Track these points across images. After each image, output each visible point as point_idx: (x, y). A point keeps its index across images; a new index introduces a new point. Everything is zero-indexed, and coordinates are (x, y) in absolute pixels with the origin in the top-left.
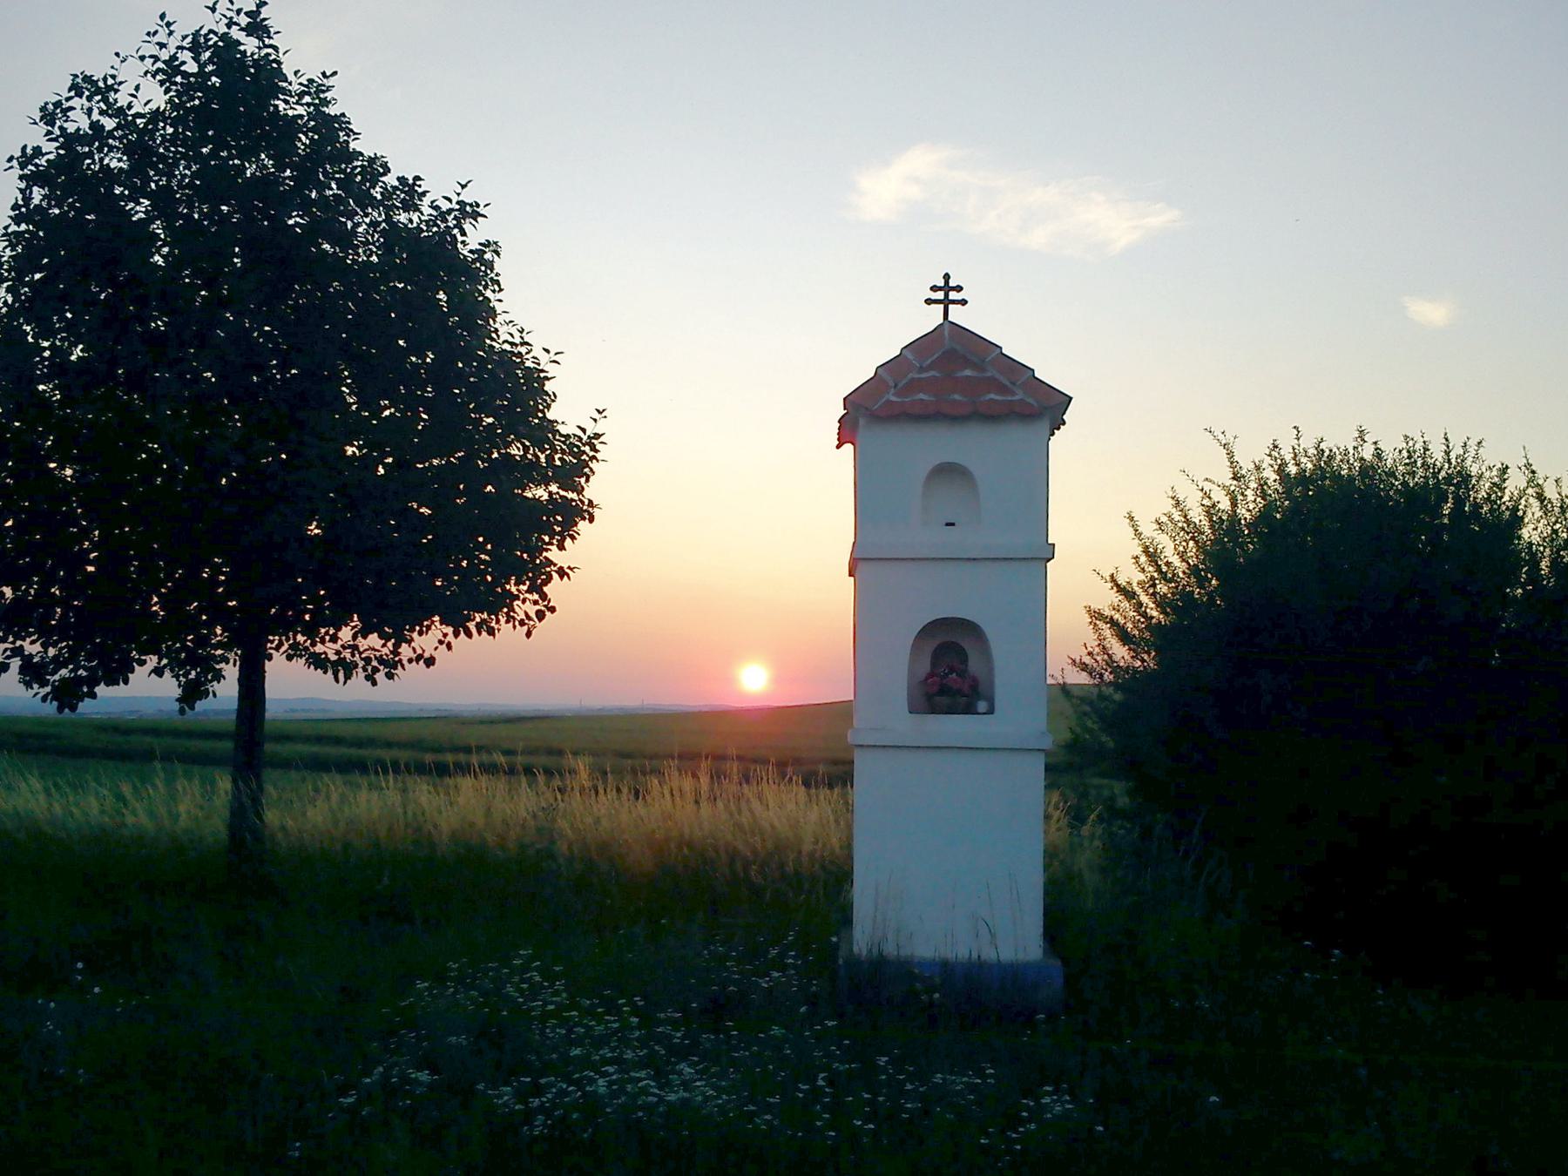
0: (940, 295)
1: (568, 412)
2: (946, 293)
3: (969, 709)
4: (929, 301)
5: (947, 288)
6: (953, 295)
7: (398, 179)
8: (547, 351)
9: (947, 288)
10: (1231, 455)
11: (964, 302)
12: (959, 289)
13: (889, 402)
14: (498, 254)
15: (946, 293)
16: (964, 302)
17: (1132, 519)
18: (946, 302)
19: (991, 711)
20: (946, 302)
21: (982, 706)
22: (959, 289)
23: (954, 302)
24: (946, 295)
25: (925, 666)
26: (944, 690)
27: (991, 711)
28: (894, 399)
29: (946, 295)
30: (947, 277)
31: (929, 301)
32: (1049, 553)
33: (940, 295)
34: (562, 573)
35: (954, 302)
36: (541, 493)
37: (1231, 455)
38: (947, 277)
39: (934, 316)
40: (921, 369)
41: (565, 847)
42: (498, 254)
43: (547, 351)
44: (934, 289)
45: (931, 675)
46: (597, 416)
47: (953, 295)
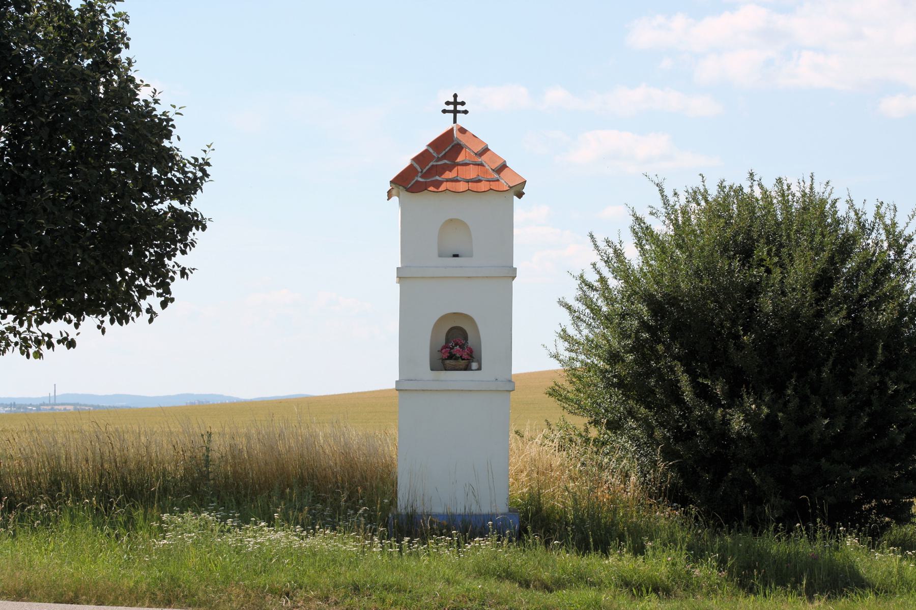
0: (451, 107)
1: (185, 143)
2: (455, 107)
3: (467, 368)
4: (444, 111)
5: (455, 103)
6: (459, 108)
7: (128, 59)
8: (174, 107)
9: (455, 103)
10: (661, 191)
11: (466, 112)
12: (463, 103)
13: (417, 181)
14: (128, 22)
15: (455, 107)
16: (466, 112)
17: (592, 236)
18: (455, 112)
19: (479, 369)
20: (455, 112)
21: (474, 365)
22: (463, 103)
23: (459, 112)
24: (455, 107)
25: (442, 341)
26: (451, 357)
27: (479, 369)
28: (420, 179)
29: (455, 107)
30: (455, 96)
31: (444, 111)
32: (512, 274)
33: (451, 107)
34: (183, 273)
35: (459, 112)
36: (162, 207)
37: (661, 191)
38: (455, 96)
39: (446, 123)
40: (439, 159)
41: (244, 441)
42: (128, 22)
43: (174, 107)
44: (448, 103)
45: (445, 347)
46: (206, 149)
47: (459, 108)
